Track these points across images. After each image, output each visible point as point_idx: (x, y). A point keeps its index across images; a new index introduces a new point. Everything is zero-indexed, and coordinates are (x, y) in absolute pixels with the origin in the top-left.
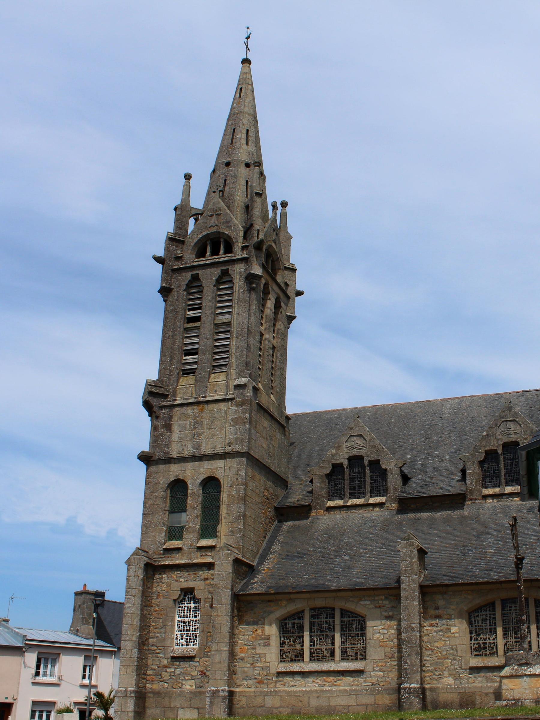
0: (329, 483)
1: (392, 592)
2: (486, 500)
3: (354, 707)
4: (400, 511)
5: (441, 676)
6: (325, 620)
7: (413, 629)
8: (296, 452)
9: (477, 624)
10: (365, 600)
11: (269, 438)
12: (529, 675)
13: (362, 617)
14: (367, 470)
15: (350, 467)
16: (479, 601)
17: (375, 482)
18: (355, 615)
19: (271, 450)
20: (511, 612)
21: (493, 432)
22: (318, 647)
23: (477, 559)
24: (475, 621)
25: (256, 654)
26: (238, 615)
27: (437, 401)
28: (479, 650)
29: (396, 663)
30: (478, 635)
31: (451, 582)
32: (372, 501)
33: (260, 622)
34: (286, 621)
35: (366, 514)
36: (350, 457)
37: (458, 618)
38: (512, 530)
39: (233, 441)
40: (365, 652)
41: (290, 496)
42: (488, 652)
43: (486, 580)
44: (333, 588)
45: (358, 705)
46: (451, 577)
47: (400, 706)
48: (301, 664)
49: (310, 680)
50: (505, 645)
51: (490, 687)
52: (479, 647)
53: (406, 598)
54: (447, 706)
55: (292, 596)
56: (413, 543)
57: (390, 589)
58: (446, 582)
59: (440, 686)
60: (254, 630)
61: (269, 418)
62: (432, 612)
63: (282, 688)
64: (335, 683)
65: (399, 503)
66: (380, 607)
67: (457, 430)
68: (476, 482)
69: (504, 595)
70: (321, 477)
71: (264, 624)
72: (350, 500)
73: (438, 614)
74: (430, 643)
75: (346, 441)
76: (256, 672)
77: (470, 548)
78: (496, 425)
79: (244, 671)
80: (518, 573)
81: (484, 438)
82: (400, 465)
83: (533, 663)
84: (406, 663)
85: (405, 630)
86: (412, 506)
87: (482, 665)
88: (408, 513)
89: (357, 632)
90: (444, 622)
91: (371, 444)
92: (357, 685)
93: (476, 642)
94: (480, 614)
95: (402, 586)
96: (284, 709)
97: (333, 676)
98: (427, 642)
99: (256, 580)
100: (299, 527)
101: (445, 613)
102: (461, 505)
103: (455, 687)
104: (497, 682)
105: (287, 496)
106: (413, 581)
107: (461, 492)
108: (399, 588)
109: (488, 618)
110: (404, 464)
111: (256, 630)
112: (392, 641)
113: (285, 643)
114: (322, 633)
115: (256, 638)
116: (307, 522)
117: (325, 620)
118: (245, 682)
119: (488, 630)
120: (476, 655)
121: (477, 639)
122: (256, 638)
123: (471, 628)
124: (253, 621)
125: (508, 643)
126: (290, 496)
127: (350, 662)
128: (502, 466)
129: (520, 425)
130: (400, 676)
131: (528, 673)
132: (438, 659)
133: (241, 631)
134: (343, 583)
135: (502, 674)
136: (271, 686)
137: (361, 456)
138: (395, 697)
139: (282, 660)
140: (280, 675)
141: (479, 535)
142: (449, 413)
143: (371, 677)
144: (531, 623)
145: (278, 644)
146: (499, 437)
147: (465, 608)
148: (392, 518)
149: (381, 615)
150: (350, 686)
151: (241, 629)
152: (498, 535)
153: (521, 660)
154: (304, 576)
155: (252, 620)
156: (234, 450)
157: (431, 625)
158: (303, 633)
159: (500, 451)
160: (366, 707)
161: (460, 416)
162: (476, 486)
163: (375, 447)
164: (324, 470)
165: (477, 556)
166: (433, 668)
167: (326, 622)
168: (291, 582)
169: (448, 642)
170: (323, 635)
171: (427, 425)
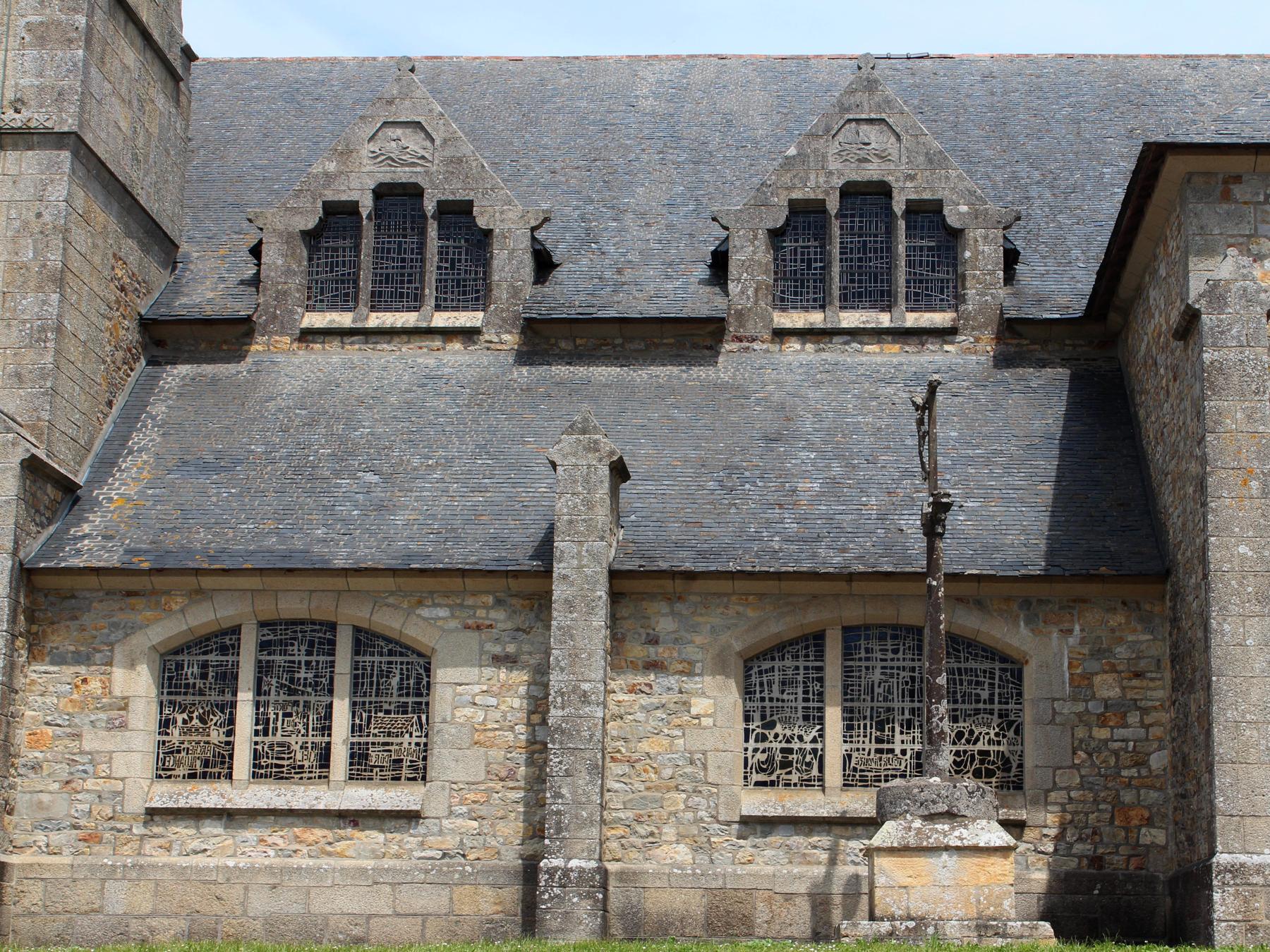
0: (310, 259)
1: (526, 586)
2: (782, 343)
3: (384, 920)
4: (526, 356)
5: (653, 839)
6: (304, 658)
7: (585, 698)
8: (196, 168)
10: (435, 605)
11: (135, 103)
12: (958, 848)
13: (420, 655)
14: (432, 231)
15: (378, 216)
16: (779, 626)
17: (453, 268)
18: (399, 647)
19: (140, 141)
20: (869, 664)
21: (815, 151)
22: (279, 738)
23: (771, 506)
24: (762, 684)
25: (82, 753)
26: (28, 632)
27: (618, 60)
28: (769, 770)
29: (521, 794)
30: (771, 725)
31: (701, 567)
32: (441, 320)
33: (98, 655)
34: (180, 658)
35: (422, 356)
36: (381, 185)
37: (713, 674)
38: (920, 422)
39: (29, 95)
40: (425, 758)
41: (185, 290)
42: (795, 778)
43: (806, 566)
44: (339, 563)
45: (398, 915)
46: (699, 553)
47: (530, 919)
48: (224, 786)
49: (250, 834)
50: (847, 758)
51: (800, 877)
52: (770, 760)
53: (570, 605)
54: (663, 928)
55: (207, 582)
56: (596, 442)
57: (516, 574)
58: (688, 566)
59: (649, 867)
60: (78, 681)
61: (139, 41)
62: (637, 651)
63: (162, 858)
64: (329, 848)
65: (523, 332)
66: (478, 628)
67: (685, 143)
68: (756, 290)
69: (854, 614)
70: (288, 237)
71: (110, 664)
72: (374, 314)
73: (653, 657)
74: (625, 740)
75: (371, 139)
76: (80, 807)
77: (747, 474)
78: (827, 130)
79: (41, 802)
80: (931, 549)
81: (788, 163)
82: (533, 223)
83: (967, 813)
84: (558, 795)
85: (559, 700)
86: (563, 344)
87: (779, 812)
88: (550, 364)
89: (404, 699)
90: (672, 681)
91: (448, 152)
92: (398, 856)
93: (761, 746)
94: (777, 664)
95: (558, 568)
96: (166, 922)
97: (323, 827)
98: (619, 738)
99: (86, 528)
100: (214, 381)
101: (675, 655)
102: (707, 352)
103: (694, 874)
104: (820, 863)
105: (175, 289)
106: (594, 556)
107: (714, 314)
108: (548, 573)
109: (800, 678)
110: (546, 220)
111: (85, 681)
112: (512, 728)
113: (175, 722)
114: (293, 698)
115: (82, 706)
116: (243, 367)
117: (304, 658)
118: (41, 838)
119: (800, 714)
120: (758, 784)
121: (764, 738)
122: (82, 706)
123: (749, 704)
124: (77, 653)
125: (855, 754)
126: (185, 290)
127: (378, 786)
128: (836, 251)
130: (535, 832)
131: (955, 842)
132: (648, 789)
133: (33, 682)
134: (367, 552)
135: (879, 839)
136: (126, 849)
137: (416, 185)
138: (512, 894)
139: (163, 772)
140: (157, 818)
141: (769, 439)
142: (657, 96)
143: (441, 833)
145: (154, 726)
146: (833, 165)
147: (738, 646)
148: (504, 374)
149: (482, 652)
150: (376, 857)
151: (34, 676)
152: (825, 442)
153: (934, 802)
154: (239, 522)
155: (72, 648)
156: (33, 124)
157: (632, 690)
158: (235, 694)
159: (833, 205)
160: (424, 922)
161: (688, 107)
162: (756, 303)
163: (460, 160)
164: (297, 218)
165: (772, 498)
166: (630, 814)
167: (308, 663)
168: (200, 541)
169: (681, 741)
170: (296, 703)
171: (594, 123)
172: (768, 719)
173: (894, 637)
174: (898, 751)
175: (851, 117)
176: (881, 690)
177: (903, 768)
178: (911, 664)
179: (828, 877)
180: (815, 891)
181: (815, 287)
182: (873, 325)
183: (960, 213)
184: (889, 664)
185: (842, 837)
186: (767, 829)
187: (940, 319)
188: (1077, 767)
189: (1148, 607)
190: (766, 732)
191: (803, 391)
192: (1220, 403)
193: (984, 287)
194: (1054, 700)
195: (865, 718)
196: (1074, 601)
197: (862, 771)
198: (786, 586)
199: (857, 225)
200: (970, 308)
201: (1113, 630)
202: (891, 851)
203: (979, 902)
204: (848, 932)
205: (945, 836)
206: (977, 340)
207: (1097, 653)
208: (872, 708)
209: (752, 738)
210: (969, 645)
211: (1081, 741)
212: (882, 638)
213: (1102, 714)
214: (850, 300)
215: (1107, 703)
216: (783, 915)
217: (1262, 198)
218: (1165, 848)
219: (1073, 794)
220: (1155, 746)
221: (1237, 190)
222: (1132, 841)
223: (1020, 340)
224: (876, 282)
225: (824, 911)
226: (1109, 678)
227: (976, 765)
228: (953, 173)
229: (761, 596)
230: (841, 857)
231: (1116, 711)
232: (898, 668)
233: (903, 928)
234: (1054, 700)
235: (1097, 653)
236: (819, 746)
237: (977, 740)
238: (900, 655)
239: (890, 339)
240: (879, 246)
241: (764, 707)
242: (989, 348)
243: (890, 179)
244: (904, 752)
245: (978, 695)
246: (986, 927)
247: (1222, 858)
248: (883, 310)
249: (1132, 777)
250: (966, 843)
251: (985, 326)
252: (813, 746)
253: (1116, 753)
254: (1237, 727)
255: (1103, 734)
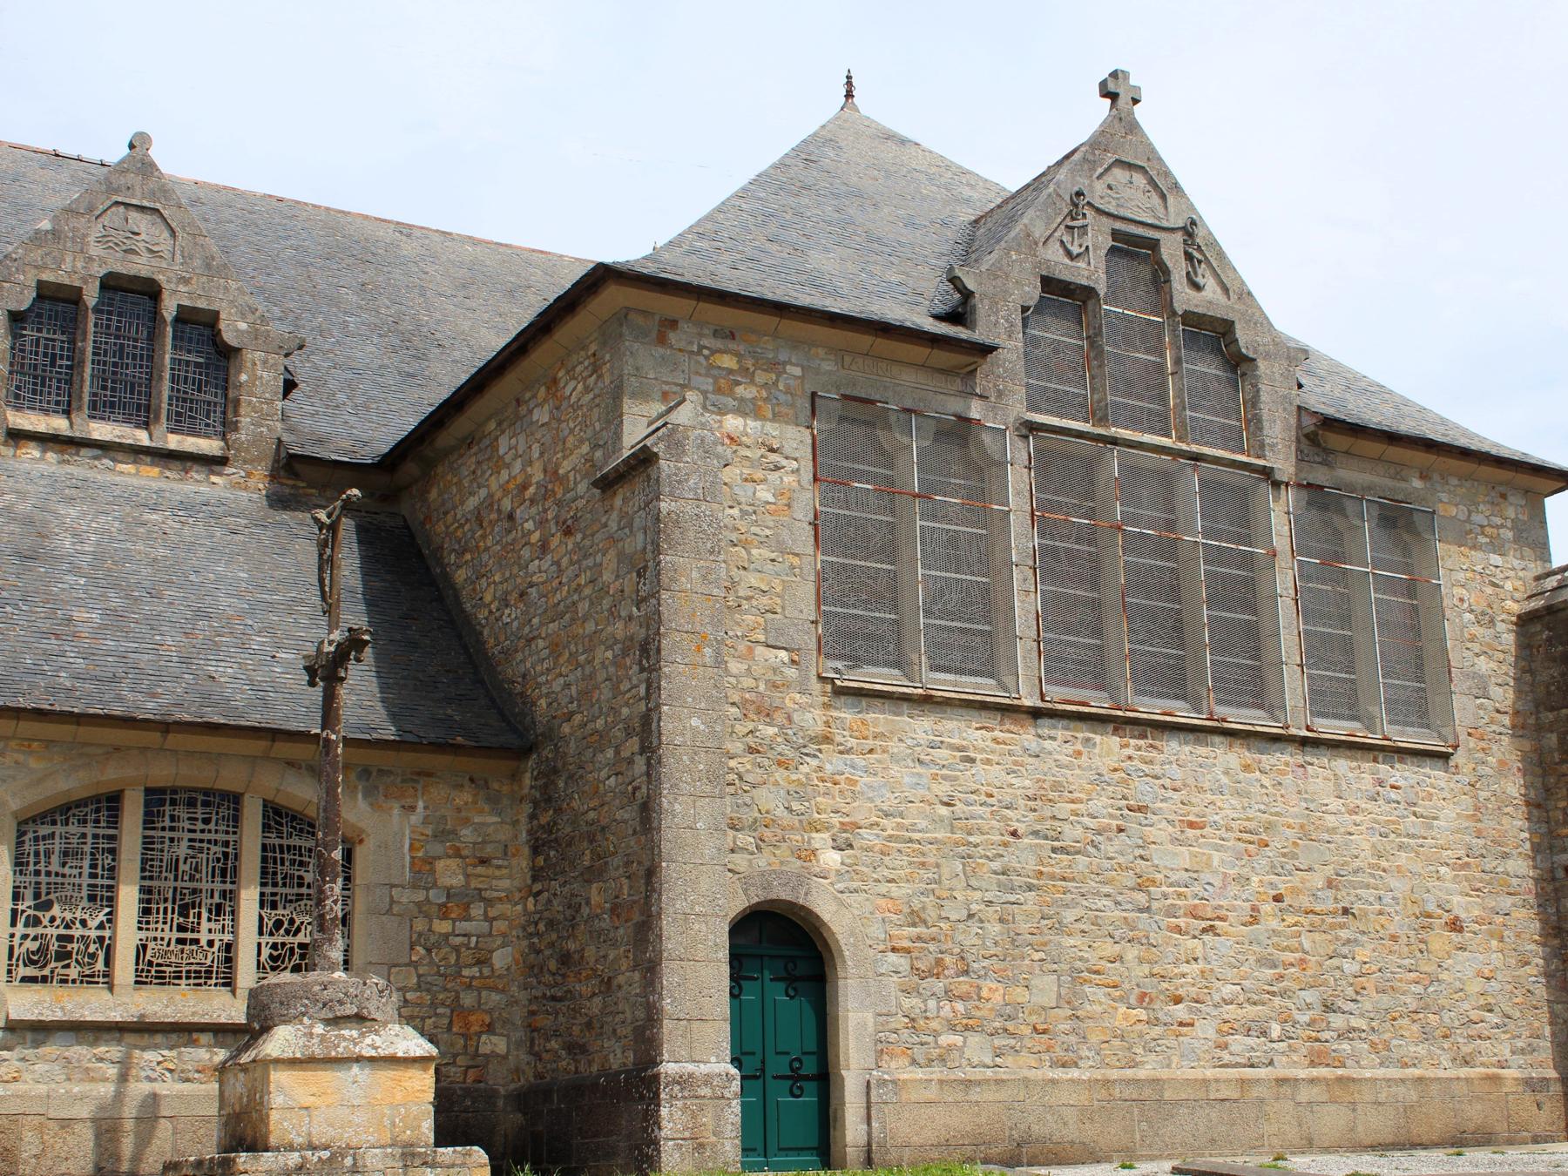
2: (17, 447)
9: (42, 867)
12: (372, 1059)
16: (70, 782)
21: (74, 230)
23: (46, 634)
24: (37, 854)
28: (42, 963)
30: (47, 906)
38: (323, 545)
42: (73, 972)
51: (82, 1098)
52: (43, 950)
69: (163, 773)
78: (91, 210)
81: (38, 238)
87: (59, 1016)
93: (32, 931)
94: (59, 829)
109: (87, 848)
119: (85, 893)
120: (24, 979)
121: (37, 922)
125: (151, 945)
129: (173, 232)
144: (243, 881)
147: (15, 804)
153: (341, 1003)
159: (91, 296)
172: (44, 898)
173: (206, 804)
174: (203, 942)
175: (120, 199)
176: (187, 868)
177: (208, 962)
178: (225, 837)
179: (119, 1097)
180: (101, 1115)
181: (59, 388)
182: (130, 441)
183: (238, 330)
184: (198, 836)
185: (136, 1047)
186: (40, 1037)
187: (209, 446)
188: (415, 964)
189: (496, 786)
190: (40, 914)
191: (53, 506)
192: (676, 559)
193: (261, 417)
194: (393, 886)
195: (166, 900)
196: (419, 774)
197: (159, 965)
198: (84, 732)
199: (114, 324)
200: (243, 437)
201: (459, 810)
202: (293, 1063)
203: (393, 1124)
204: (248, 1167)
205: (356, 1044)
206: (249, 475)
207: (441, 835)
208: (175, 889)
209: (21, 921)
210: (294, 818)
211: (420, 935)
212: (191, 803)
213: (444, 905)
214: (101, 408)
215: (449, 892)
216: (57, 1146)
217: (695, 348)
218: (505, 1057)
219: (409, 996)
220: (499, 942)
221: (673, 337)
222: (471, 1050)
223: (299, 476)
224: (132, 393)
225: (111, 1140)
226: (453, 863)
227: (296, 959)
228: (233, 285)
229: (49, 743)
230: (134, 1072)
231: (458, 902)
232: (209, 842)
233: (315, 1159)
234: (393, 886)
235: (441, 835)
236: (107, 933)
237: (298, 930)
238: (212, 826)
239: (148, 459)
240: (138, 352)
241: (38, 883)
242: (261, 486)
243: (160, 278)
244: (211, 943)
245: (301, 877)
246: (413, 1155)
247: (668, 1068)
248: (138, 426)
249: (473, 978)
250: (382, 1053)
251: (258, 460)
252: (100, 933)
253: (457, 949)
254: (686, 920)
255: (443, 927)
